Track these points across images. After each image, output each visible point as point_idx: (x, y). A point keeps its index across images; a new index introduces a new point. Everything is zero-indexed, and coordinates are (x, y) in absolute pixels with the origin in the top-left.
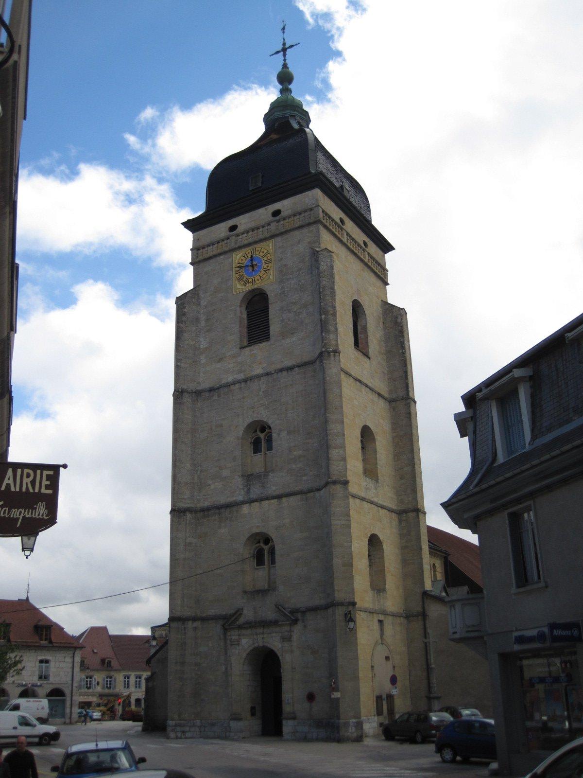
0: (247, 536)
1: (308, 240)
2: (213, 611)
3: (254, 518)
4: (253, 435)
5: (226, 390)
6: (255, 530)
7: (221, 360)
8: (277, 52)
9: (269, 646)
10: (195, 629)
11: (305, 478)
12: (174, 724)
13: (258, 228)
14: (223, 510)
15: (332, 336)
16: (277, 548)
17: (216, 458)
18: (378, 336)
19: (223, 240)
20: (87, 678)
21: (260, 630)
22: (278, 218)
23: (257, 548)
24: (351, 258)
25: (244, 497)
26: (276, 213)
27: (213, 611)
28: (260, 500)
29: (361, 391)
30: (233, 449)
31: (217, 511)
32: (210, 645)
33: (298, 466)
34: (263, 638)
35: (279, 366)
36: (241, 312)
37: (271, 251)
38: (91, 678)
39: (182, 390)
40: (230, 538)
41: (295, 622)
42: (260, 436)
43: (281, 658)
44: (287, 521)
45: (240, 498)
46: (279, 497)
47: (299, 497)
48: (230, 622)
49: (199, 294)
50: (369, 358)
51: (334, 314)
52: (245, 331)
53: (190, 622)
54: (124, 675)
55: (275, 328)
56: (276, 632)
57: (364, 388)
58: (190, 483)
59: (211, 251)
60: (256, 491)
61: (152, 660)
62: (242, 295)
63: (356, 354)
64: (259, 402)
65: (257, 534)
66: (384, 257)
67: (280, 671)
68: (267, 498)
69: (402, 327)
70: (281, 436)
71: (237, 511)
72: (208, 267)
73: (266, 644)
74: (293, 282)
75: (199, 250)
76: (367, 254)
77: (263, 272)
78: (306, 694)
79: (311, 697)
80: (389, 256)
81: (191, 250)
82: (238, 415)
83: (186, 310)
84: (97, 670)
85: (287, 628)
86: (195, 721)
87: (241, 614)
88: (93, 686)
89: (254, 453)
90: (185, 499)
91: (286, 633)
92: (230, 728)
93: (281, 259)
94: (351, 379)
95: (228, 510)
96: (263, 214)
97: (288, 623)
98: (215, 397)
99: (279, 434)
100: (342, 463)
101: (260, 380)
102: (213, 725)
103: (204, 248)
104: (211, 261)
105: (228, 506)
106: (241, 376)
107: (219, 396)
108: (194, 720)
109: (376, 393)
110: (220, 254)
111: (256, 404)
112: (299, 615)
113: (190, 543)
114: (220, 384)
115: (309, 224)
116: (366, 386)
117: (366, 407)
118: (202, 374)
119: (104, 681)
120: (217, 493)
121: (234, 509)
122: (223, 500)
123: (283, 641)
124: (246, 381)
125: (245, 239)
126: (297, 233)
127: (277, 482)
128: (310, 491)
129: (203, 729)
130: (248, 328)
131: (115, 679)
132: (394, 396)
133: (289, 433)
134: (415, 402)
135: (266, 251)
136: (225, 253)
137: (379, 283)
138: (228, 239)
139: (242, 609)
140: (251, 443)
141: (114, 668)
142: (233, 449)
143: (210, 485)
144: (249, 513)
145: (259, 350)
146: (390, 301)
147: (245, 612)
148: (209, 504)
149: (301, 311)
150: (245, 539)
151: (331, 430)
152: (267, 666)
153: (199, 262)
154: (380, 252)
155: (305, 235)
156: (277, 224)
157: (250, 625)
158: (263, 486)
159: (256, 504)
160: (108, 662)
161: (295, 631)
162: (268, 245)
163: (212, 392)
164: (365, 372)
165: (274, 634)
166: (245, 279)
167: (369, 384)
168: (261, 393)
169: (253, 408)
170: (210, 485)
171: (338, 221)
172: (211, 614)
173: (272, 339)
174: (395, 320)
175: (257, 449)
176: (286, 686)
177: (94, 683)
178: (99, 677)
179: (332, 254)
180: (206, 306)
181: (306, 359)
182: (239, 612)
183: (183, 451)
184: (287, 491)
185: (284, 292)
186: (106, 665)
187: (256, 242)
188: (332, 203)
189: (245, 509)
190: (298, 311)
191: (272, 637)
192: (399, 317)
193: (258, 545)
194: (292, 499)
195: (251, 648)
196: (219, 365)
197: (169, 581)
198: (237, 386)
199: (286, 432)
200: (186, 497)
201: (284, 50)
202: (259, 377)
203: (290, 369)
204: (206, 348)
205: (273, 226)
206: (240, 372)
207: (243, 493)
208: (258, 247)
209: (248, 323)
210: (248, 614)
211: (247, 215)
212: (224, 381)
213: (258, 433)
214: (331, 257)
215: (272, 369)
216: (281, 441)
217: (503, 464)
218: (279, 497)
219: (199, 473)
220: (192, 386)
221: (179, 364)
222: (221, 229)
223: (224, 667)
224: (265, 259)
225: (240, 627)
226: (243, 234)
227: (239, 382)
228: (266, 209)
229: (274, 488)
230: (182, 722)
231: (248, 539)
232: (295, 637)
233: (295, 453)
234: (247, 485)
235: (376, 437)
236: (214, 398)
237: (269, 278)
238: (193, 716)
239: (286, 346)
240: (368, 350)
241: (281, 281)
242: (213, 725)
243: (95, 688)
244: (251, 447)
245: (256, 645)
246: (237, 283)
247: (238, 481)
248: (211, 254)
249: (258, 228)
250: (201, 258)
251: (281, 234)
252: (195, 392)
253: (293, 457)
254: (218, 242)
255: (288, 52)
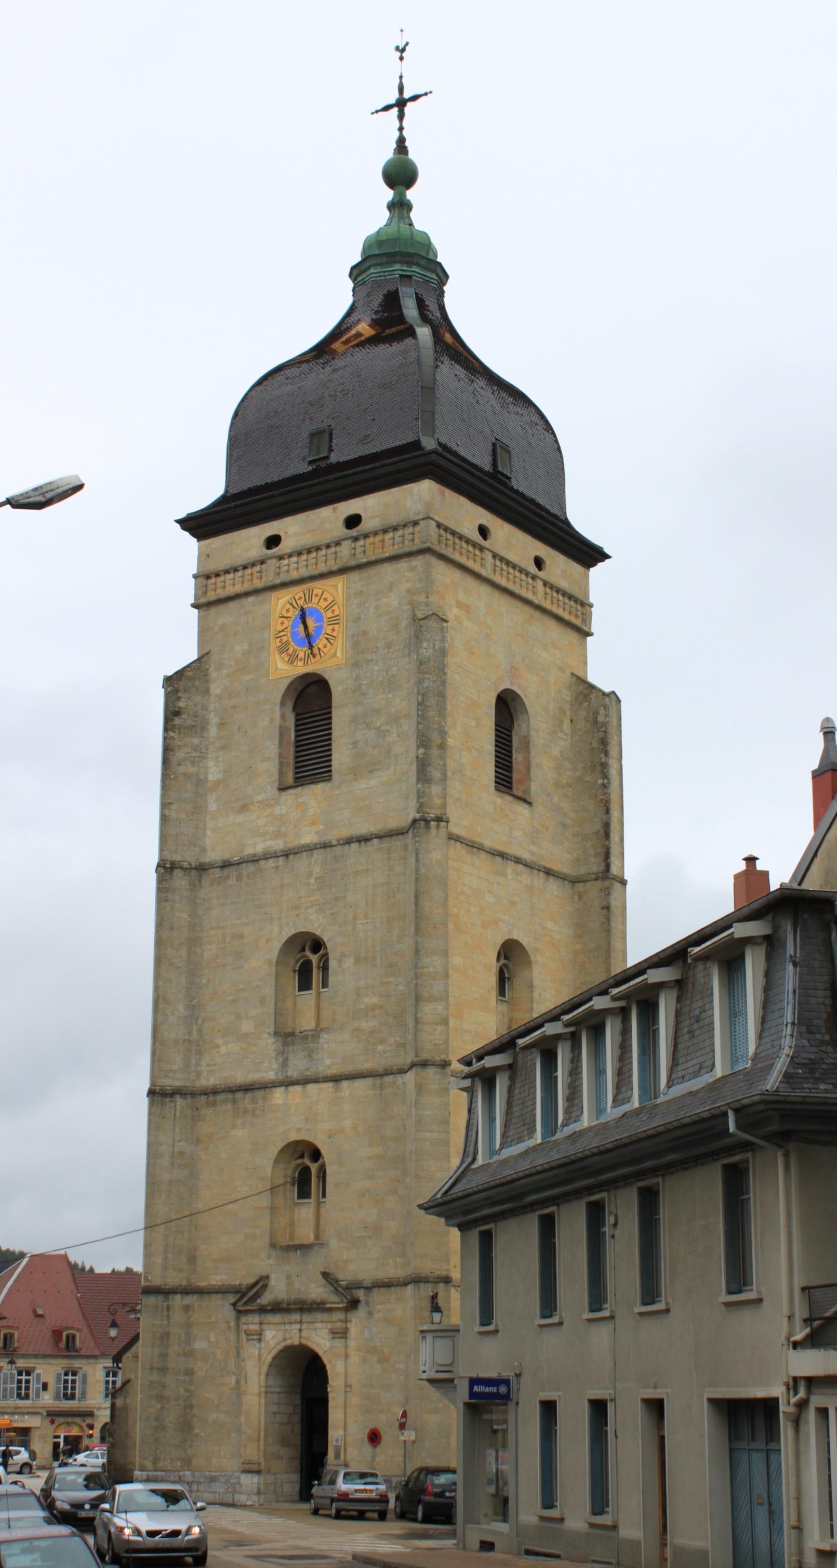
0: (280, 1146)
1: (408, 585)
2: (218, 1278)
3: (295, 1114)
4: (299, 956)
5: (251, 868)
6: (294, 1136)
7: (244, 808)
8: (387, 108)
9: (310, 1344)
10: (187, 1308)
11: (380, 1048)
12: (145, 1478)
13: (318, 549)
14: (239, 1095)
15: (435, 789)
16: (329, 1170)
17: (231, 998)
18: (556, 752)
19: (253, 565)
20: (20, 1374)
21: (296, 1317)
22: (354, 532)
23: (299, 1165)
24: (502, 603)
25: (276, 1074)
26: (353, 521)
27: (218, 1278)
28: (304, 1081)
29: (504, 875)
30: (260, 983)
31: (230, 1096)
32: (212, 1339)
33: (371, 1024)
34: (300, 1330)
35: (346, 833)
36: (283, 717)
37: (340, 599)
38: (28, 1374)
39: (172, 863)
40: (245, 1152)
41: (354, 1304)
42: (307, 959)
43: (328, 1367)
44: (348, 1123)
45: (271, 1075)
46: (336, 1079)
47: (369, 1081)
48: (249, 1299)
49: (207, 670)
50: (530, 804)
51: (442, 746)
52: (292, 750)
53: (178, 1297)
54: (105, 1368)
55: (340, 756)
56: (322, 1322)
57: (511, 867)
58: (184, 1041)
59: (232, 585)
60: (298, 1065)
61: (125, 1356)
62: (286, 683)
63: (499, 801)
64: (309, 896)
65: (297, 1143)
66: (587, 576)
67: (326, 1388)
68: (316, 1081)
69: (605, 732)
70: (344, 966)
71: (264, 1099)
72: (226, 616)
73: (304, 1342)
74: (376, 668)
75: (208, 577)
76: (540, 584)
77: (325, 641)
78: (368, 1431)
79: (374, 1438)
80: (597, 572)
81: (195, 577)
82: (272, 920)
83: (181, 704)
84: (45, 1356)
85: (340, 1316)
86: (182, 1473)
87: (265, 1286)
88: (31, 1392)
89: (300, 990)
90: (174, 1071)
91: (339, 1324)
92: (241, 1485)
93: (358, 618)
94: (483, 855)
95: (249, 1095)
96: (327, 520)
97: (340, 1306)
98: (232, 882)
99: (340, 962)
100: (440, 1028)
101: (312, 855)
102: (213, 1479)
103: (217, 575)
104: (232, 605)
105: (248, 1088)
106: (279, 845)
107: (239, 878)
108: (179, 1471)
109: (539, 870)
110: (247, 594)
111: (303, 900)
112: (360, 1294)
113: (182, 1153)
114: (242, 855)
115: (410, 554)
116: (518, 861)
117: (513, 903)
118: (209, 832)
119: (58, 1381)
120: (226, 1063)
121: (260, 1094)
122: (241, 1077)
123: (333, 1338)
124: (286, 854)
125: (296, 568)
126: (387, 568)
127: (334, 1052)
128: (388, 1072)
129: (195, 1487)
130: (297, 747)
131: (85, 1376)
132: (583, 871)
133: (357, 961)
134: (624, 883)
135: (330, 599)
136: (256, 592)
137: (572, 636)
138: (262, 562)
139: (267, 1277)
140: (294, 971)
141: (82, 1353)
142: (260, 983)
143: (218, 1046)
144: (285, 1104)
145: (313, 796)
146: (593, 678)
147: (273, 1282)
148: (217, 1082)
149: (388, 728)
150: (276, 1152)
151: (423, 967)
152: (306, 1377)
153: (209, 604)
154: (577, 568)
155: (404, 576)
156: (353, 545)
157: (277, 1308)
158: (310, 1056)
159: (297, 1089)
160: (68, 1337)
161: (354, 1320)
162: (336, 587)
163: (226, 871)
164: (518, 833)
165: (319, 1325)
166: (291, 651)
167: (526, 856)
168: (312, 881)
169: (297, 908)
170: (218, 1046)
171: (477, 537)
172: (214, 1283)
173: (335, 775)
174: (596, 718)
175: (305, 983)
176: (335, 1415)
177: (34, 1386)
178: (48, 1371)
179: (445, 624)
180: (219, 697)
181: (394, 823)
182: (262, 1283)
183: (171, 981)
184: (349, 1068)
185: (360, 685)
186: (63, 1344)
187: (313, 578)
188: (463, 501)
189: (278, 1095)
190: (384, 728)
191: (315, 1329)
192: (602, 711)
193: (300, 1161)
194: (358, 1083)
195: (280, 1347)
196: (240, 818)
197: (142, 1225)
198: (271, 863)
199: (352, 960)
200: (175, 1067)
201: (401, 104)
202: (309, 849)
203: (363, 840)
204: (218, 782)
205: (345, 549)
206: (278, 835)
207: (275, 1065)
208: (318, 587)
209: (297, 736)
210: (278, 1289)
211: (300, 517)
212: (249, 851)
213: (308, 953)
214: (443, 630)
215: (332, 836)
216: (343, 971)
217: (483, 1166)
218: (336, 1079)
219: (200, 1021)
220: (189, 856)
221: (167, 812)
222: (248, 541)
223: (233, 1379)
224: (329, 614)
225: (263, 1310)
226: (290, 556)
227: (275, 856)
228: (334, 510)
229: (328, 1062)
230: (160, 1473)
231: (282, 1151)
232: (353, 1329)
233: (366, 1000)
234: (283, 1053)
235: (532, 959)
236: (229, 882)
237: (335, 655)
238: (179, 1463)
239: (366, 789)
240: (530, 786)
241: (356, 665)
242: (213, 1479)
243: (38, 1396)
244: (294, 979)
245: (289, 1342)
246: (277, 657)
247: (269, 1044)
248: (230, 590)
249: (318, 549)
250: (212, 596)
251: (360, 567)
252: (196, 868)
253: (363, 1007)
254: (245, 568)
255: (409, 108)
